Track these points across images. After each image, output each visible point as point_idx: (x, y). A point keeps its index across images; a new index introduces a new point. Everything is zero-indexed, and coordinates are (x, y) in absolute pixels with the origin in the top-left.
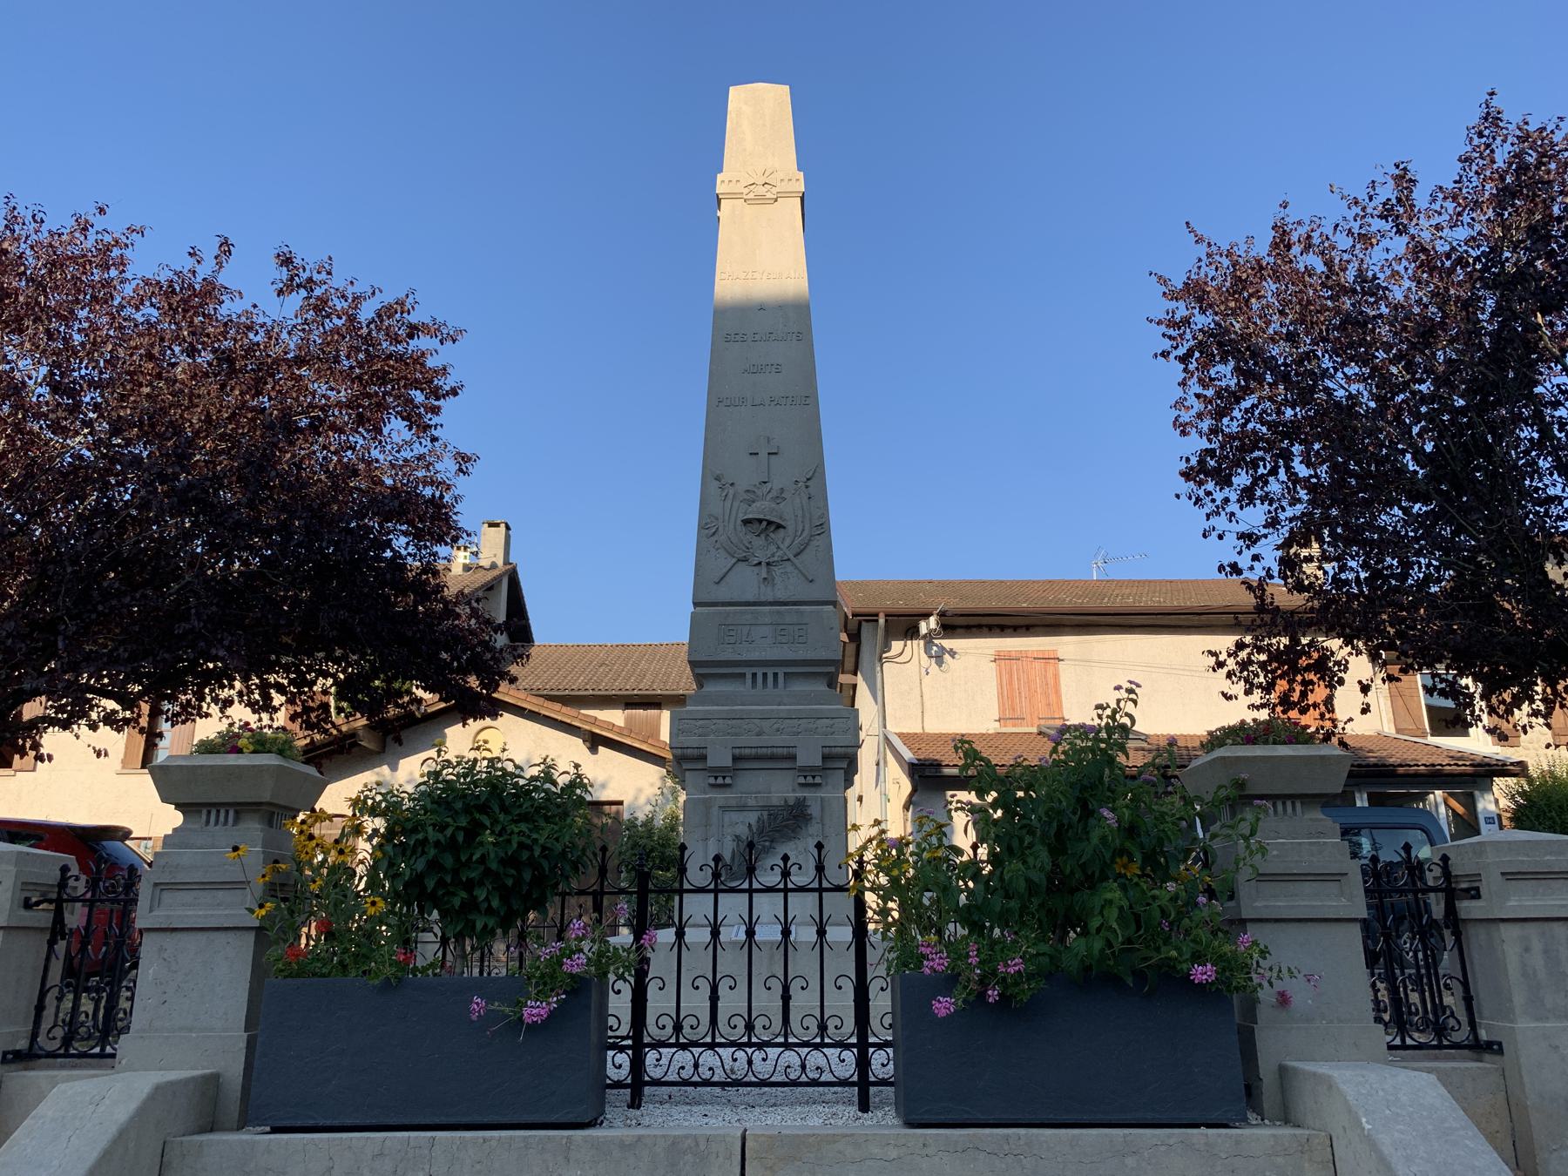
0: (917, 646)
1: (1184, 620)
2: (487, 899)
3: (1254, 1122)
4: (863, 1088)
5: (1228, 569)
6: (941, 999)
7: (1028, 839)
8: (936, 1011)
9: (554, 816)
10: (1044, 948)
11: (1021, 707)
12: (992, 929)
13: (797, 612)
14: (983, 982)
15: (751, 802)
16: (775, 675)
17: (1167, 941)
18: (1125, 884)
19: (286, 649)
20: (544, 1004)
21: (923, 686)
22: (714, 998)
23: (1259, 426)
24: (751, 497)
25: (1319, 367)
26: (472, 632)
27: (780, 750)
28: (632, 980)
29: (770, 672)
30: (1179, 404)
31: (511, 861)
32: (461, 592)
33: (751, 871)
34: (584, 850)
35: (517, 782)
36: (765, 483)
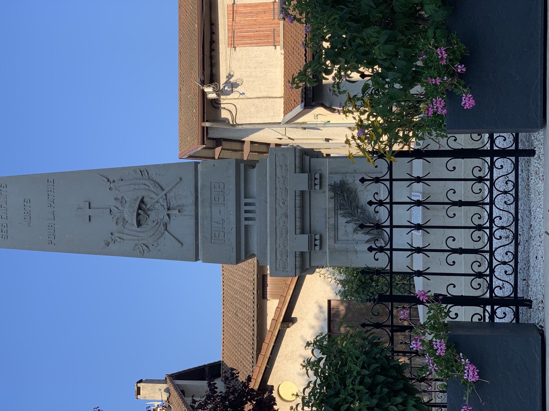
0: (225, 101)
2: (396, 406)
6: (463, 103)
7: (358, 41)
8: (471, 106)
10: (430, 33)
11: (266, 31)
12: (417, 67)
14: (452, 74)
15: (332, 221)
16: (246, 204)
20: (466, 367)
21: (251, 97)
24: (122, 221)
27: (298, 202)
28: (449, 306)
31: (371, 389)
33: (378, 226)
34: (364, 339)
35: (319, 385)
36: (111, 211)
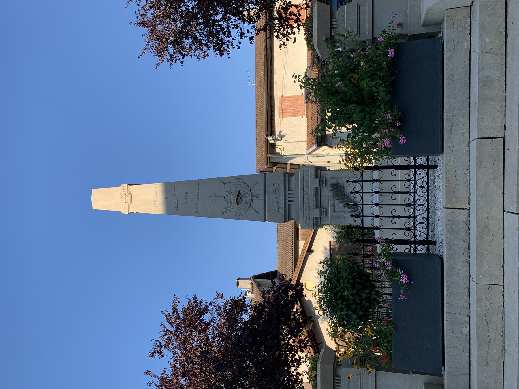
0: (278, 144)
1: (269, 55)
2: (366, 294)
3: (442, 35)
4: (430, 167)
5: (252, 41)
8: (404, 143)
9: (338, 271)
10: (382, 107)
11: (298, 109)
12: (375, 124)
13: (268, 187)
14: (394, 127)
15: (332, 202)
16: (289, 194)
17: (380, 65)
18: (361, 79)
19: (280, 354)
22: (399, 217)
23: (205, 31)
25: (184, 11)
26: (275, 293)
27: (314, 192)
28: (393, 244)
29: (288, 196)
30: (198, 57)
31: (353, 286)
32: (262, 296)
33: (356, 204)
34: (349, 261)
35: (326, 283)
36: (225, 197)
